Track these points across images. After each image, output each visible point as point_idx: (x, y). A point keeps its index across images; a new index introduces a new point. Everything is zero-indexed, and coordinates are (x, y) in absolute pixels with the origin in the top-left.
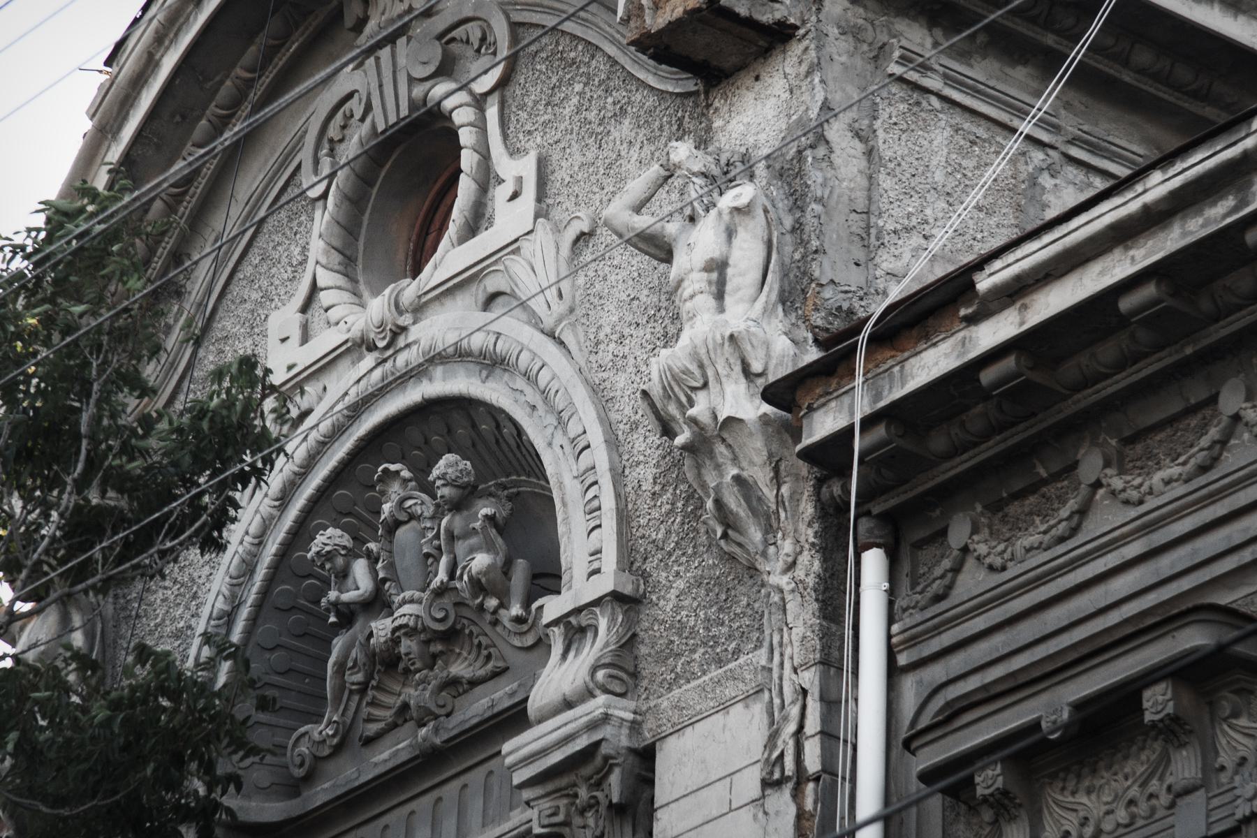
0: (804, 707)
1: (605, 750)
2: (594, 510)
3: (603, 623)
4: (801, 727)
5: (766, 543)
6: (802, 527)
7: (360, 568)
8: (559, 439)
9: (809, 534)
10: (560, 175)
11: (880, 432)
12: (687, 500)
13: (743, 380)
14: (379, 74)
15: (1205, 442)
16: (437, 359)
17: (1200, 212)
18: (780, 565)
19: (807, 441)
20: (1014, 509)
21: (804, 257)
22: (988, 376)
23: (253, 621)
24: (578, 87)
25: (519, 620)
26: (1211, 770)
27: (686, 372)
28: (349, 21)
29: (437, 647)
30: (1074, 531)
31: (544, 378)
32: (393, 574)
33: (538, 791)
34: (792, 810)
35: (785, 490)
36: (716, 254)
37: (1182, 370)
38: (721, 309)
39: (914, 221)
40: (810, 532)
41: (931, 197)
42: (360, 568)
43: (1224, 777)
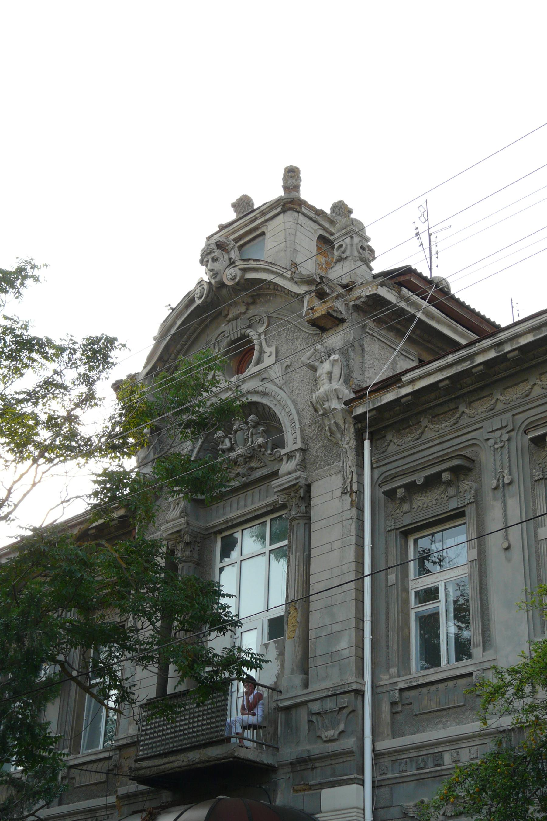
0: (352, 476)
1: (300, 484)
2: (294, 428)
3: (298, 455)
4: (352, 480)
5: (342, 438)
6: (351, 434)
7: (227, 441)
8: (283, 412)
9: (353, 436)
10: (281, 351)
11: (374, 412)
12: (319, 427)
13: (337, 400)
14: (233, 327)
15: (455, 418)
16: (249, 392)
17: (461, 364)
18: (345, 443)
19: (354, 414)
20: (403, 432)
21: (349, 372)
22: (403, 400)
23: (198, 452)
24: (286, 332)
25: (270, 454)
26: (458, 492)
27: (323, 397)
28: (223, 314)
29: (247, 460)
30: (420, 437)
31: (279, 398)
32: (236, 443)
33: (281, 493)
34: (350, 499)
35: (346, 425)
36: (330, 370)
37: (450, 400)
38: (331, 383)
39: (372, 366)
40: (353, 436)
41: (375, 360)
42: (227, 441)
43: (461, 494)
